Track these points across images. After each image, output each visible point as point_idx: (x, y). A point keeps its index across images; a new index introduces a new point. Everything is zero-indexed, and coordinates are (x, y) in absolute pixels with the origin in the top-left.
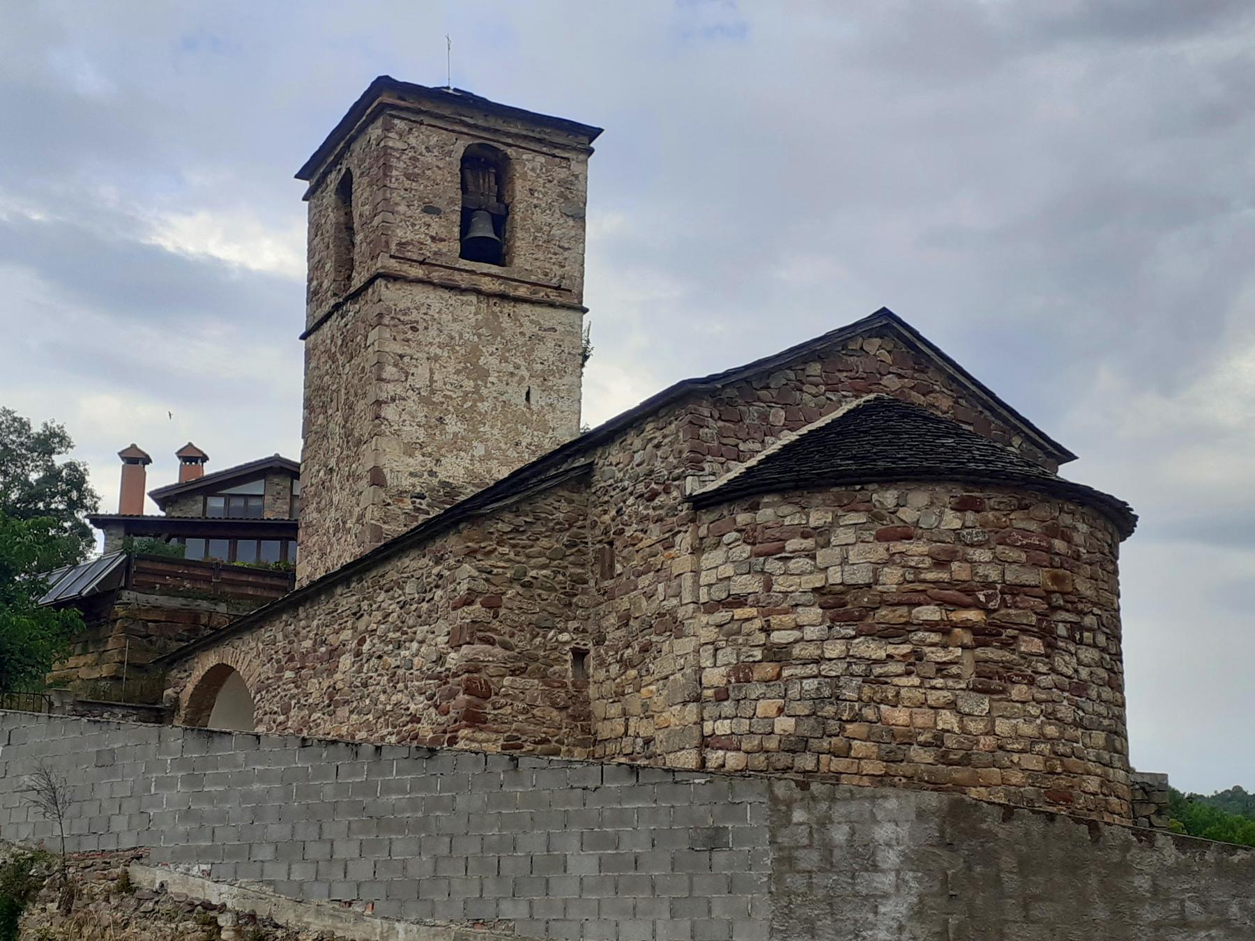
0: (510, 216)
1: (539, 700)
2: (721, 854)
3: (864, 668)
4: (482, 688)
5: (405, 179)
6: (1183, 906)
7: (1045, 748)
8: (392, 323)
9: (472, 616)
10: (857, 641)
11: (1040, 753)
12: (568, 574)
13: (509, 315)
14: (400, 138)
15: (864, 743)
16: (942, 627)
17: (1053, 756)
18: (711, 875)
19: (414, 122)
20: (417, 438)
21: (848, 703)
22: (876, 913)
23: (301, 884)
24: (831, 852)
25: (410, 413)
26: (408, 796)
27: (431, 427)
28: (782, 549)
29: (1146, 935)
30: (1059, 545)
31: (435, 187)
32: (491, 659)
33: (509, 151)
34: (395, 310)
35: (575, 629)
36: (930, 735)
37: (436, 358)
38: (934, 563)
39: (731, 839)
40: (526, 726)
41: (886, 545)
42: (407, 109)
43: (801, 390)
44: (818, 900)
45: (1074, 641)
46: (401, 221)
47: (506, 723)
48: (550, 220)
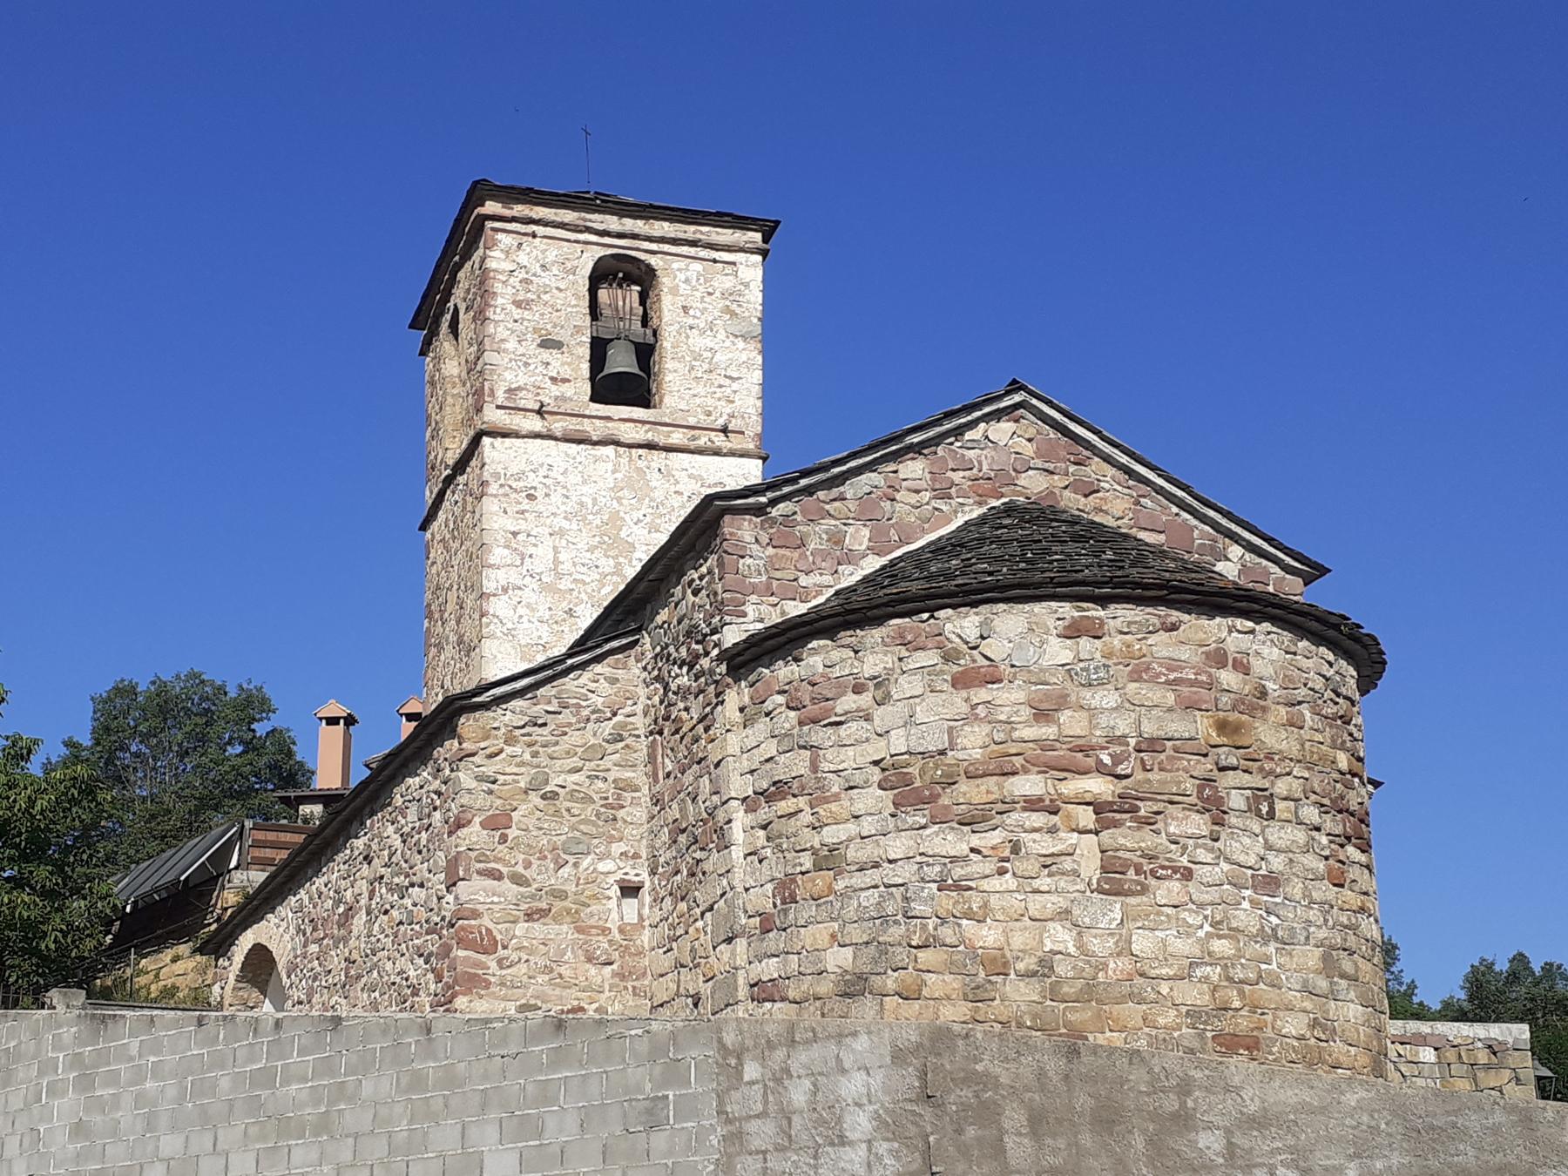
0: (658, 344)
1: (569, 953)
3: (939, 869)
4: (482, 940)
5: (514, 308)
8: (501, 491)
9: (467, 842)
10: (928, 831)
11: (1205, 979)
12: (610, 780)
13: (660, 470)
14: (507, 257)
16: (1047, 802)
17: (1225, 983)
18: (649, 1165)
19: (525, 234)
21: (919, 920)
25: (528, 606)
26: (310, 1084)
28: (830, 712)
31: (555, 313)
32: (496, 899)
33: (653, 261)
34: (505, 475)
35: (622, 854)
36: (1034, 960)
37: (561, 533)
38: (1034, 714)
39: (671, 1113)
40: (548, 990)
41: (964, 694)
42: (513, 220)
43: (893, 500)
46: (511, 360)
47: (518, 987)
48: (711, 345)
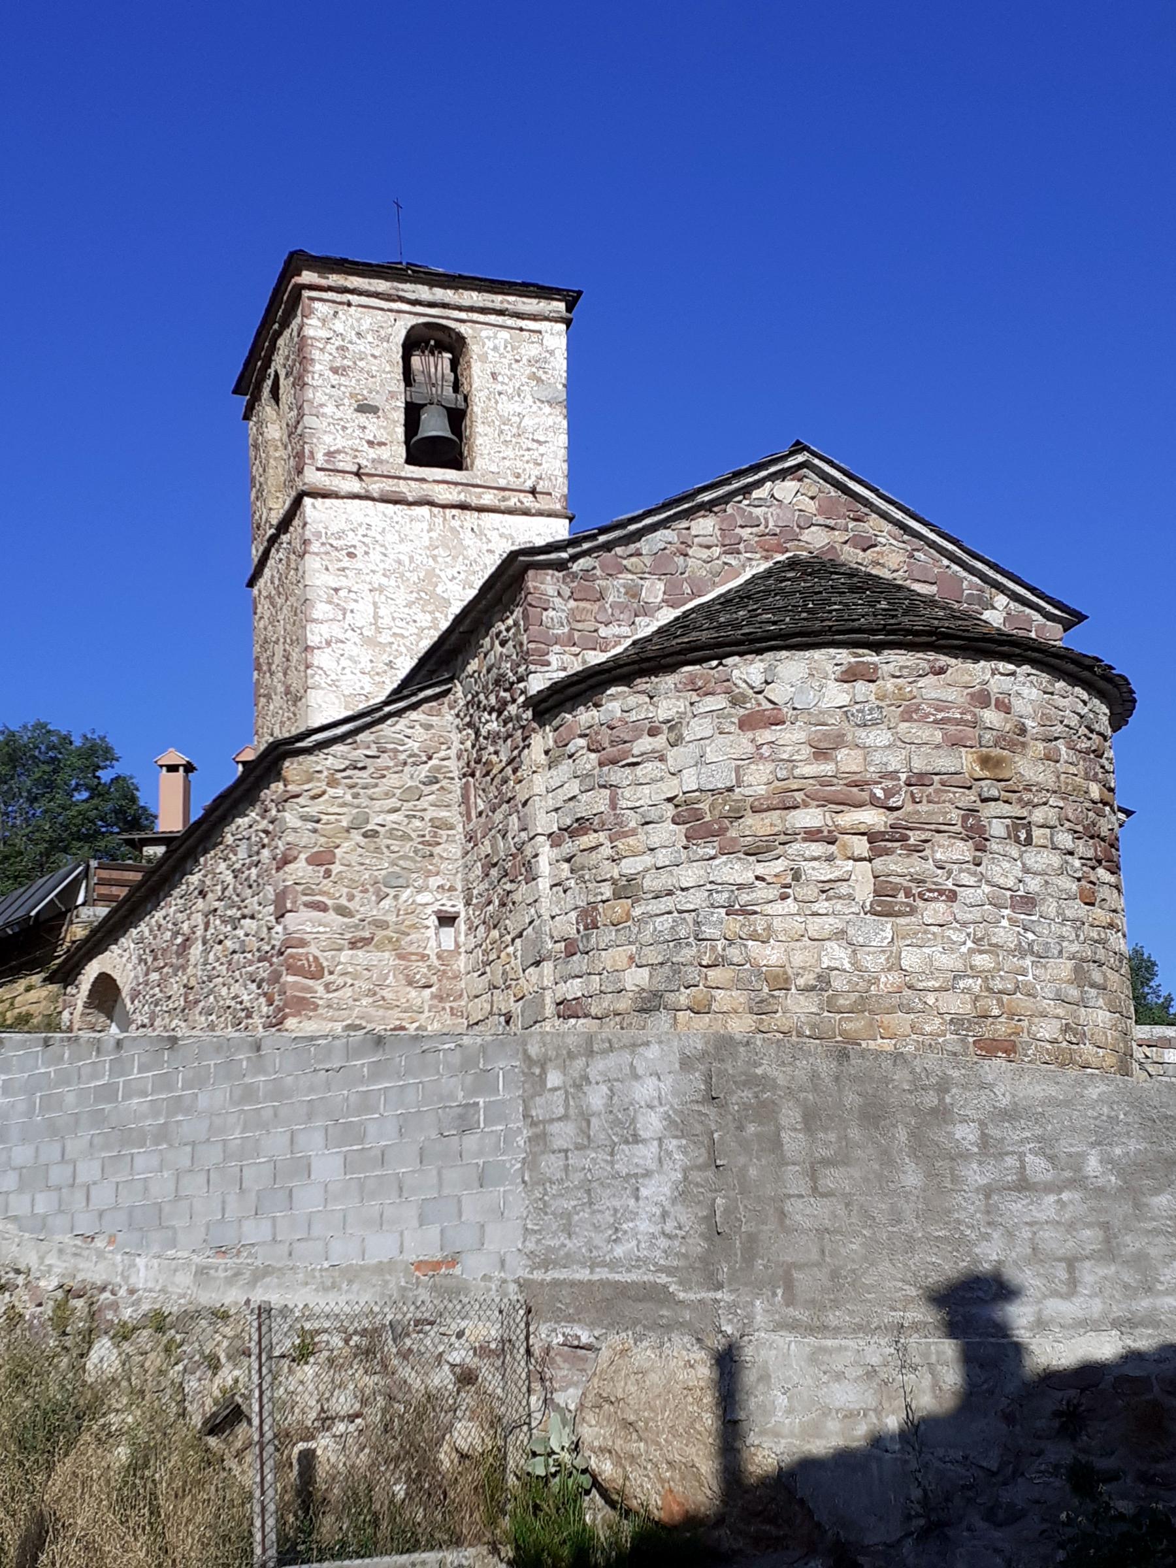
1: (391, 978)
2: (472, 1137)
4: (310, 966)
6: (1022, 1161)
7: (976, 985)
10: (717, 862)
11: (967, 990)
12: (427, 819)
15: (729, 993)
16: (826, 833)
20: (362, 688)
22: (637, 1199)
23: (45, 1217)
24: (589, 1122)
25: (351, 658)
27: (378, 674)
29: (973, 1203)
30: (991, 716)
32: (321, 929)
33: (463, 329)
36: (812, 976)
37: (381, 589)
39: (482, 1118)
40: (372, 1011)
41: (750, 735)
43: (686, 555)
44: (575, 1186)
45: (1018, 841)
48: (519, 410)
